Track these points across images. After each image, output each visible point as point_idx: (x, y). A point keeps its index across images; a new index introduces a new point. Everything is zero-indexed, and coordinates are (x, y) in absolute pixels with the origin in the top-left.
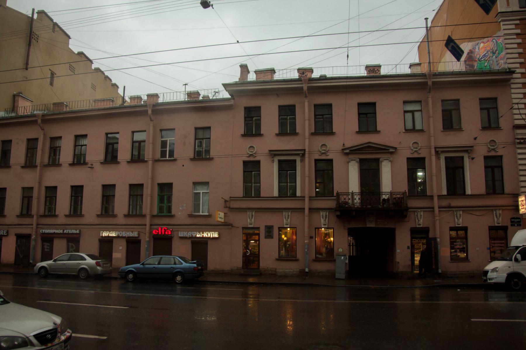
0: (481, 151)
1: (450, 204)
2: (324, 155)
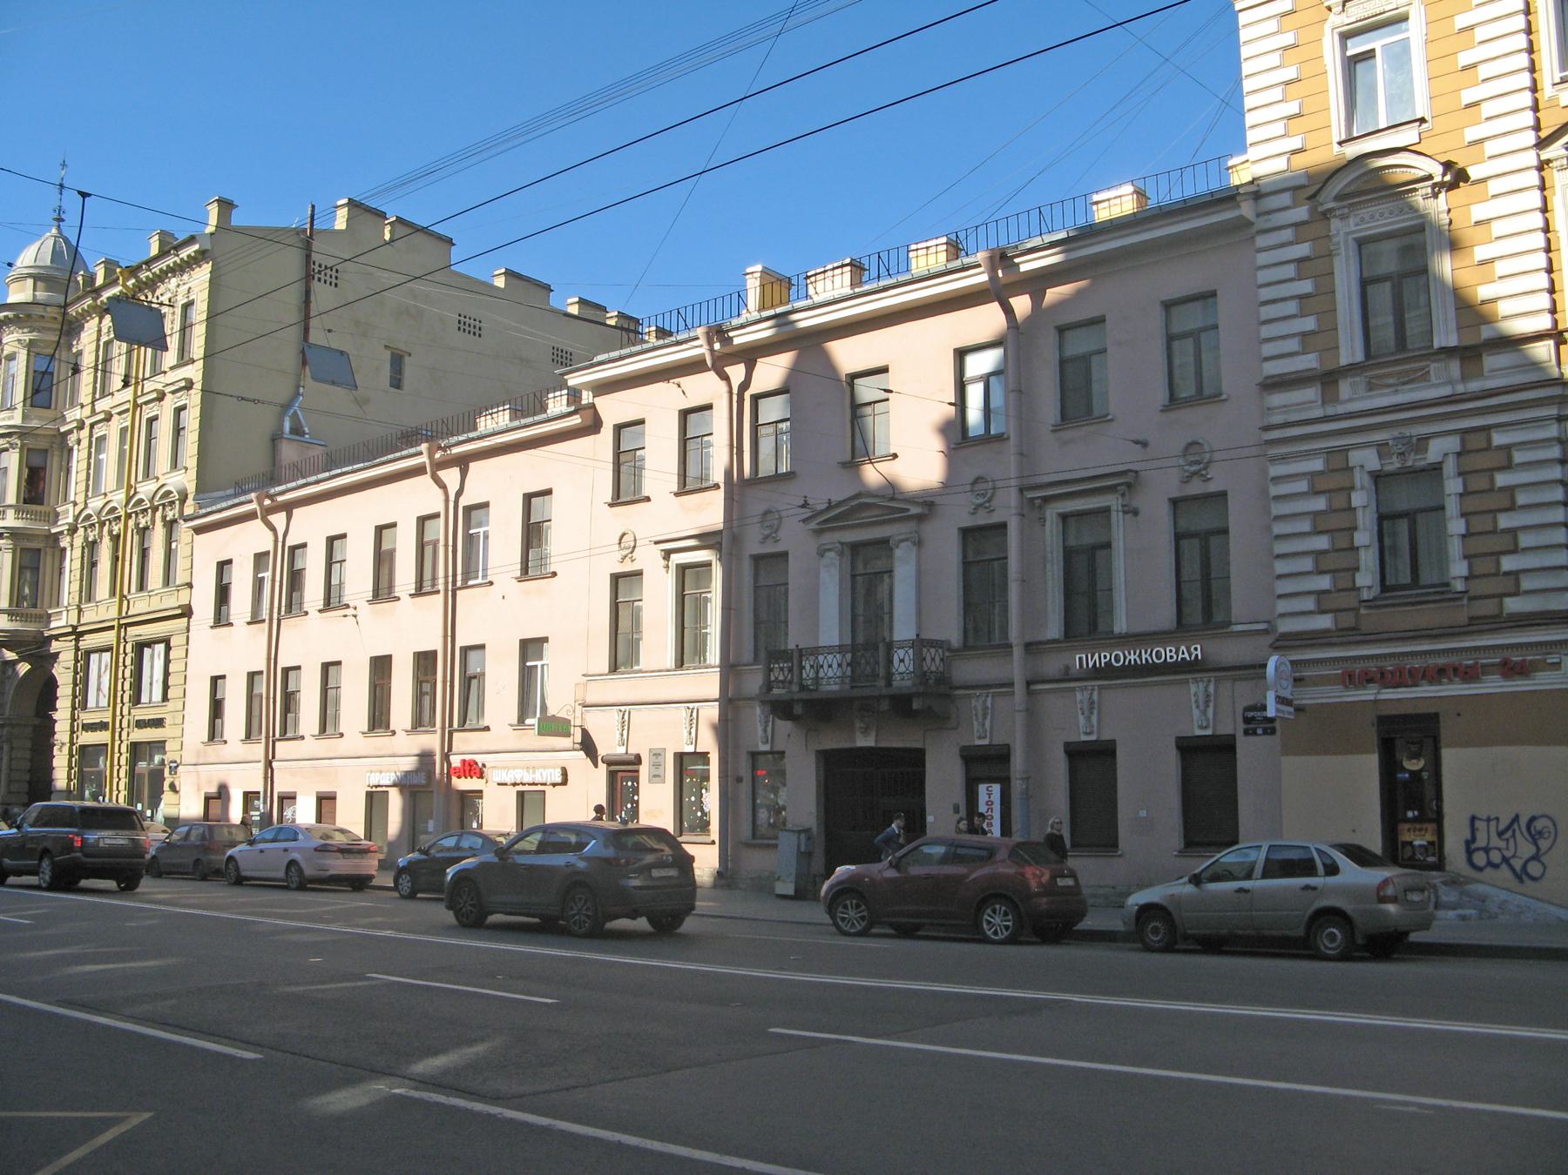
0: (1162, 485)
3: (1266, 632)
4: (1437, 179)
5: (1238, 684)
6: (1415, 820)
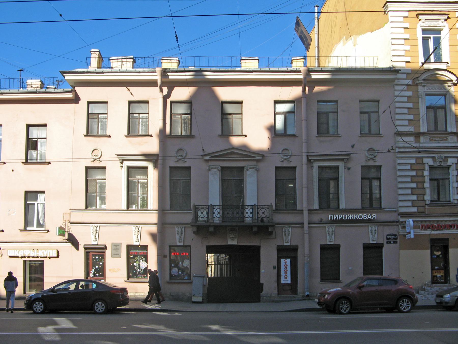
0: (359, 161)
1: (322, 219)
2: (180, 161)
3: (395, 211)
4: (454, 82)
5: (385, 227)
6: (437, 269)
